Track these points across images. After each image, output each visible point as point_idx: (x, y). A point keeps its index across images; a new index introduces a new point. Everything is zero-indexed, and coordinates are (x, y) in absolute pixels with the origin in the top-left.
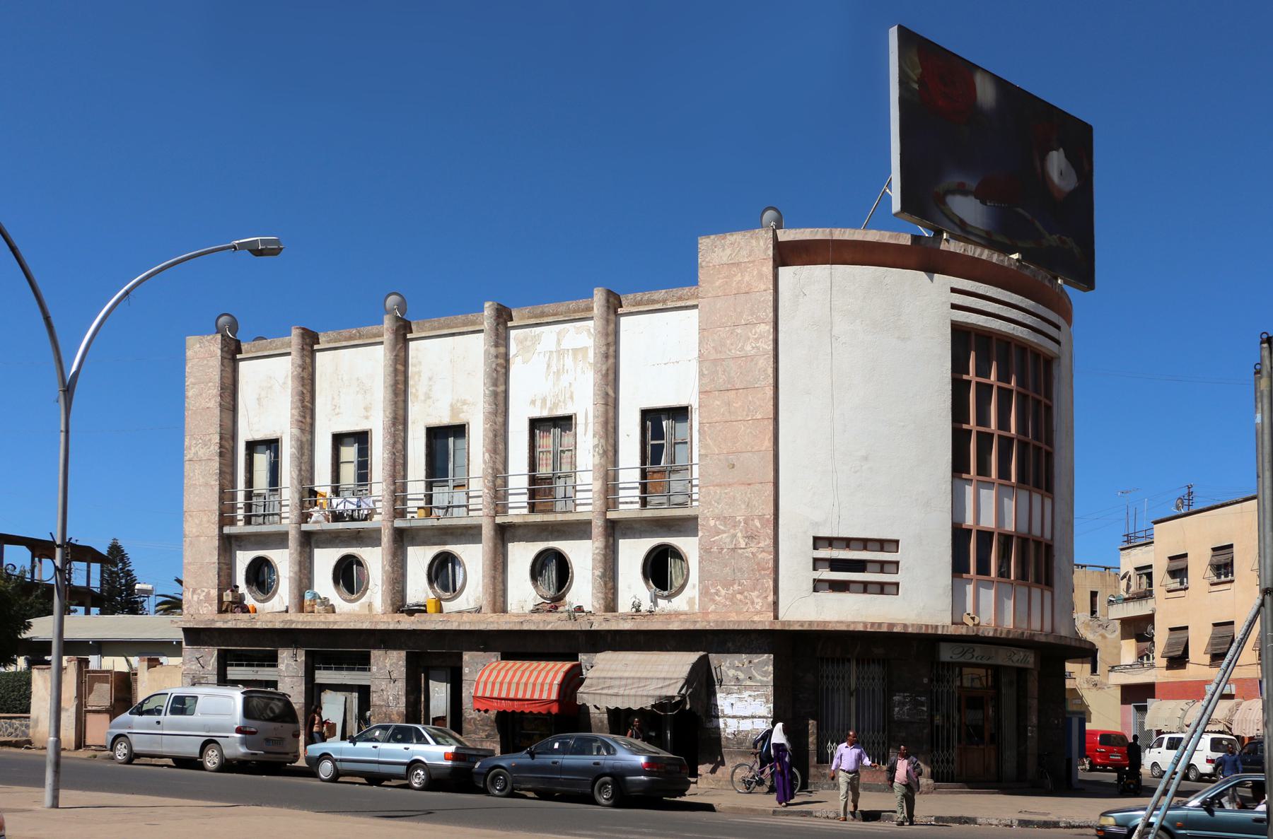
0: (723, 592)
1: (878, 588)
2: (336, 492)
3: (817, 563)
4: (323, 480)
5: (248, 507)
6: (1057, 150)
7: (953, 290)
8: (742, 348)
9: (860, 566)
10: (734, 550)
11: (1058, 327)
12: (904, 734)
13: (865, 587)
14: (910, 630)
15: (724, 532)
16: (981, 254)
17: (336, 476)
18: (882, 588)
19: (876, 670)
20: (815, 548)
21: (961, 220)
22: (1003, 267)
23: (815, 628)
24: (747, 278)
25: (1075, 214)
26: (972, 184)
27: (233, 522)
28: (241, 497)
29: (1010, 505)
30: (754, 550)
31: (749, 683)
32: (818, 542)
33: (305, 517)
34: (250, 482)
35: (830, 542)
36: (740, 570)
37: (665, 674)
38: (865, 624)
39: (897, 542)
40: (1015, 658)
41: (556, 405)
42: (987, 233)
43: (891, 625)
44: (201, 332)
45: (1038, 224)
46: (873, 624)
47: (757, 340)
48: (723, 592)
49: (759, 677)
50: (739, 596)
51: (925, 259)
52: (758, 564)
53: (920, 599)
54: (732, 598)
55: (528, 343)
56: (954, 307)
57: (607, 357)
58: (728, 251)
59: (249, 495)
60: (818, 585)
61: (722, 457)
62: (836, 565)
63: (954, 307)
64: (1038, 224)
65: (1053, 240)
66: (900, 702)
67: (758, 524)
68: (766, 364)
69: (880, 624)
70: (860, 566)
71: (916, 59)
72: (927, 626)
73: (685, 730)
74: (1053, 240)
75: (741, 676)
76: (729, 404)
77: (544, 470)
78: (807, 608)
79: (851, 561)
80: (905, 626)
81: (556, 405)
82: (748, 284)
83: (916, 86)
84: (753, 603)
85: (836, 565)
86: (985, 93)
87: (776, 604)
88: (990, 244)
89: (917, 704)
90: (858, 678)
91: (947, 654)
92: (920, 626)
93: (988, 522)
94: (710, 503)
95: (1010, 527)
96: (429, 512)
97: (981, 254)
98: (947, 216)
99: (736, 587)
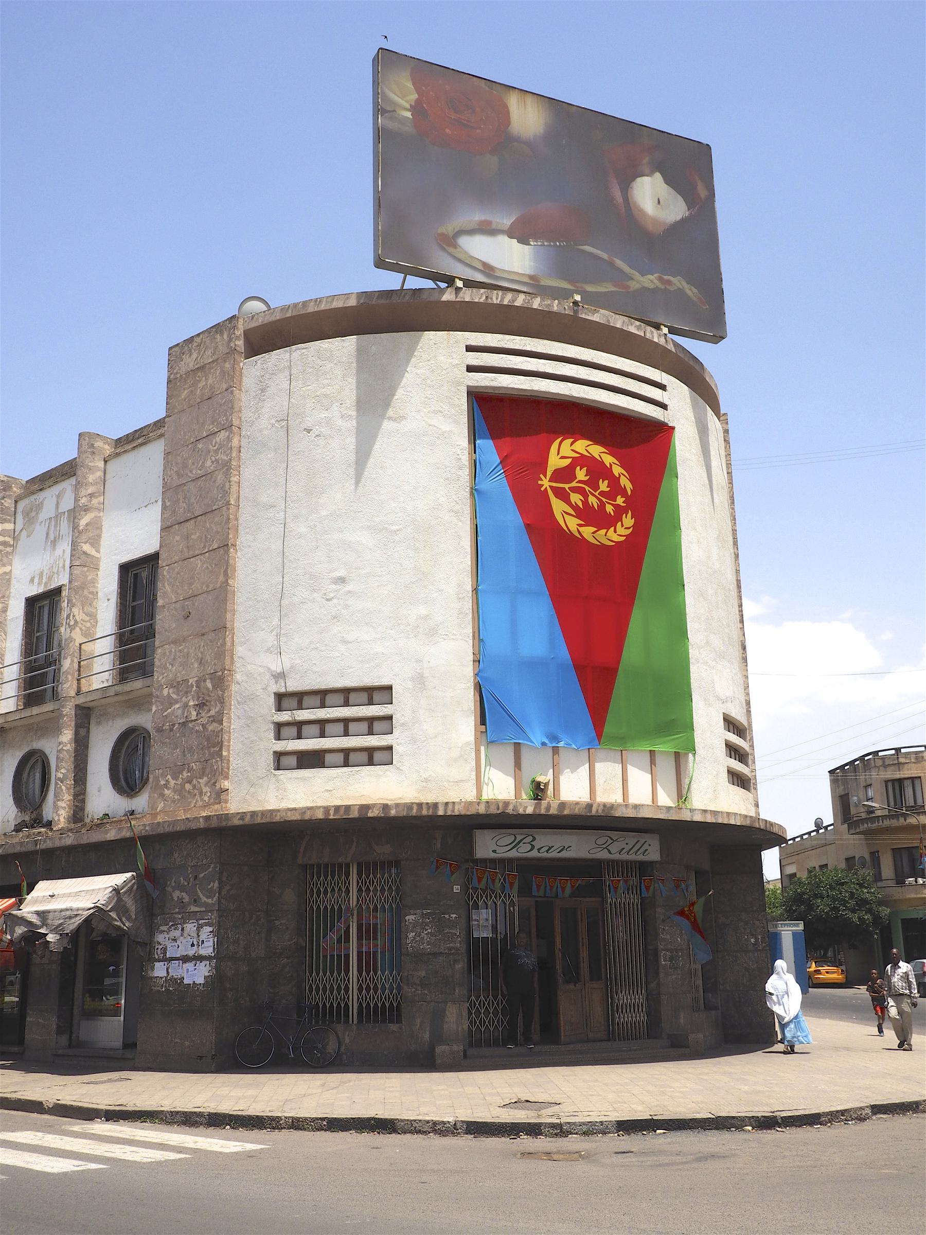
0: (172, 782)
1: (364, 757)
6: (650, 174)
7: (470, 349)
8: (203, 466)
10: (184, 724)
11: (662, 387)
12: (423, 974)
13: (347, 758)
14: (393, 812)
15: (177, 702)
16: (502, 300)
20: (279, 709)
21: (485, 264)
22: (550, 313)
23: (259, 820)
24: (210, 381)
25: (693, 249)
26: (507, 221)
30: (204, 720)
31: (193, 909)
35: (300, 698)
36: (191, 750)
38: (327, 809)
39: (390, 688)
40: (615, 848)
41: (50, 578)
42: (531, 277)
43: (365, 808)
45: (619, 263)
46: (337, 808)
47: (216, 451)
48: (172, 782)
49: (204, 899)
50: (188, 787)
52: (208, 739)
54: (180, 790)
55: (33, 514)
56: (471, 369)
58: (194, 356)
60: (279, 760)
61: (178, 605)
63: (471, 369)
64: (619, 263)
65: (650, 280)
66: (415, 924)
67: (209, 685)
69: (348, 808)
71: (410, 85)
72: (420, 805)
74: (650, 280)
75: (186, 899)
76: (187, 537)
80: (386, 807)
81: (50, 578)
82: (212, 387)
83: (408, 114)
84: (201, 794)
86: (527, 120)
90: (360, 890)
91: (487, 846)
92: (410, 806)
94: (166, 668)
97: (502, 300)
98: (460, 261)
99: (185, 774)
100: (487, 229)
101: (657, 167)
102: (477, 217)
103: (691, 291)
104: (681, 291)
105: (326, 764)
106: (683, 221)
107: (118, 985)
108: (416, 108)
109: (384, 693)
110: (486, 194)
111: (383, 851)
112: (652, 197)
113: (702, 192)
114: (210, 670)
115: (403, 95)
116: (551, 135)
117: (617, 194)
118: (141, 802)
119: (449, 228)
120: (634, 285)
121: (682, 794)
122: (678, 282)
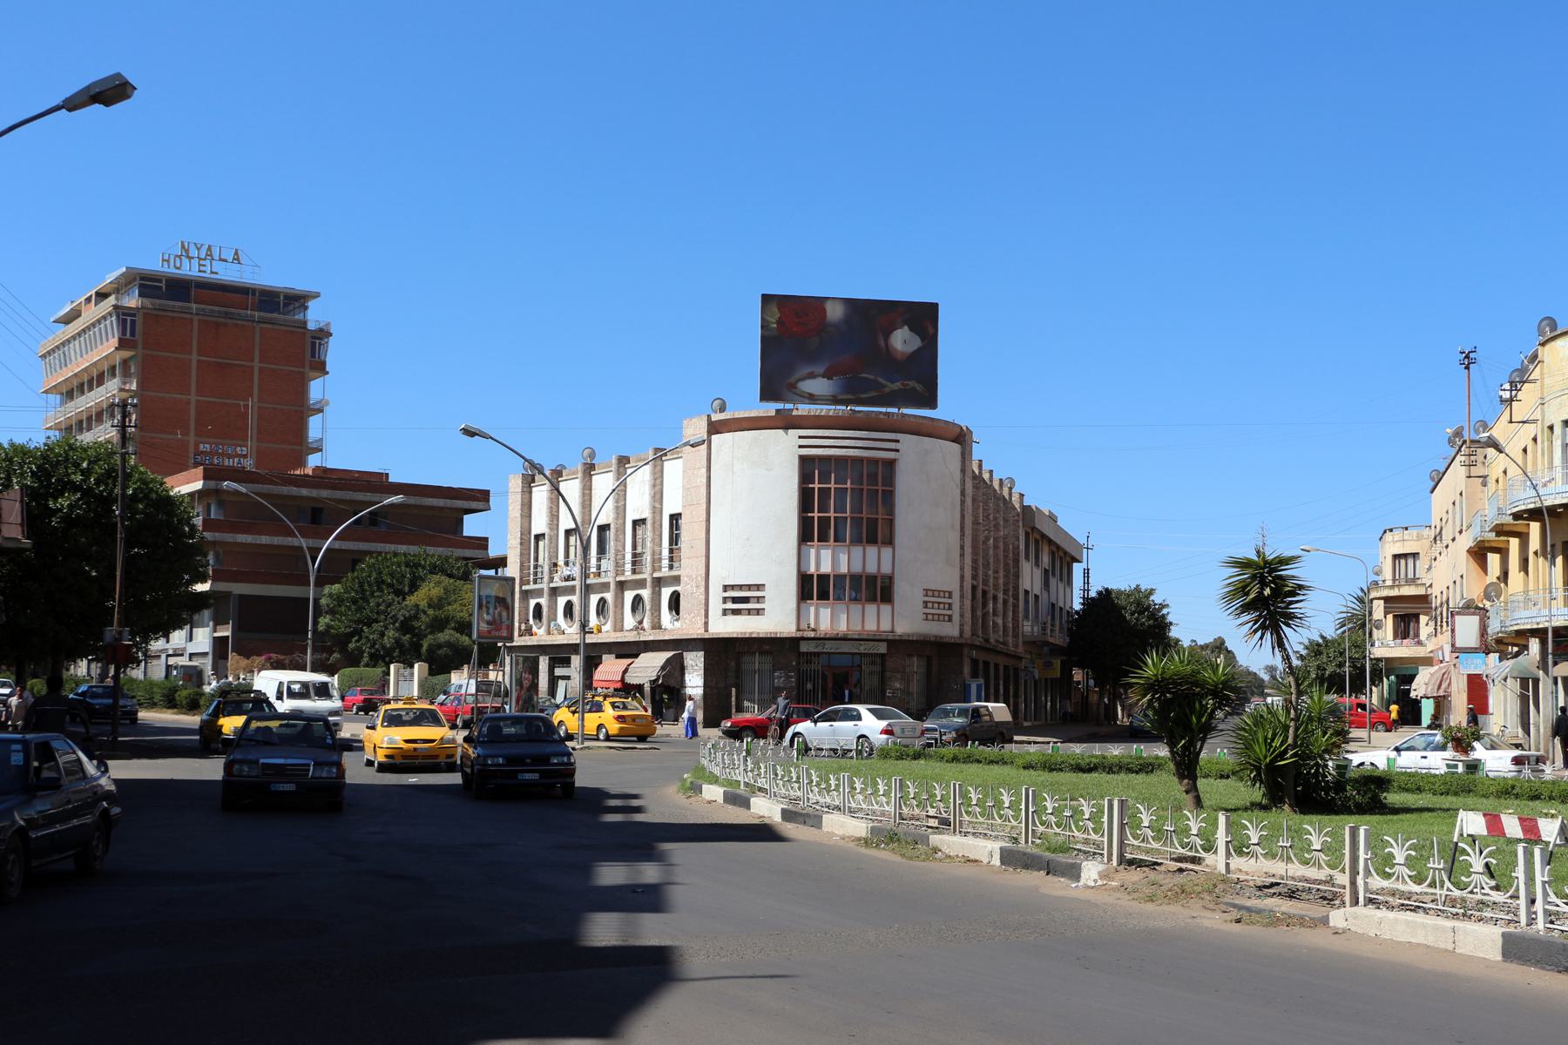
2: (567, 564)
3: (725, 600)
4: (561, 562)
5: (536, 574)
9: (746, 600)
13: (749, 612)
17: (567, 555)
18: (758, 612)
19: (769, 659)
26: (820, 369)
27: (660, 568)
28: (629, 557)
29: (843, 558)
32: (726, 588)
33: (551, 580)
34: (536, 559)
35: (733, 587)
37: (647, 668)
44: (691, 416)
51: (785, 422)
53: (778, 618)
57: (654, 486)
59: (536, 567)
60: (725, 612)
62: (735, 600)
68: (703, 490)
70: (746, 600)
73: (667, 695)
74: (897, 386)
77: (639, 550)
78: (726, 626)
79: (743, 599)
85: (735, 600)
86: (834, 313)
87: (706, 623)
88: (835, 401)
89: (788, 677)
91: (804, 648)
93: (826, 568)
95: (844, 570)
96: (599, 575)
100: (812, 376)
101: (906, 323)
102: (807, 370)
103: (919, 387)
104: (914, 389)
105: (803, 605)
106: (919, 349)
107: (129, 545)
108: (778, 322)
109: (759, 587)
110: (812, 358)
111: (766, 647)
112: (902, 340)
113: (931, 330)
114: (65, 780)
115: (774, 314)
116: (848, 319)
117: (882, 343)
118: (678, 624)
119: (792, 380)
120: (887, 390)
121: (205, 654)
122: (912, 384)
